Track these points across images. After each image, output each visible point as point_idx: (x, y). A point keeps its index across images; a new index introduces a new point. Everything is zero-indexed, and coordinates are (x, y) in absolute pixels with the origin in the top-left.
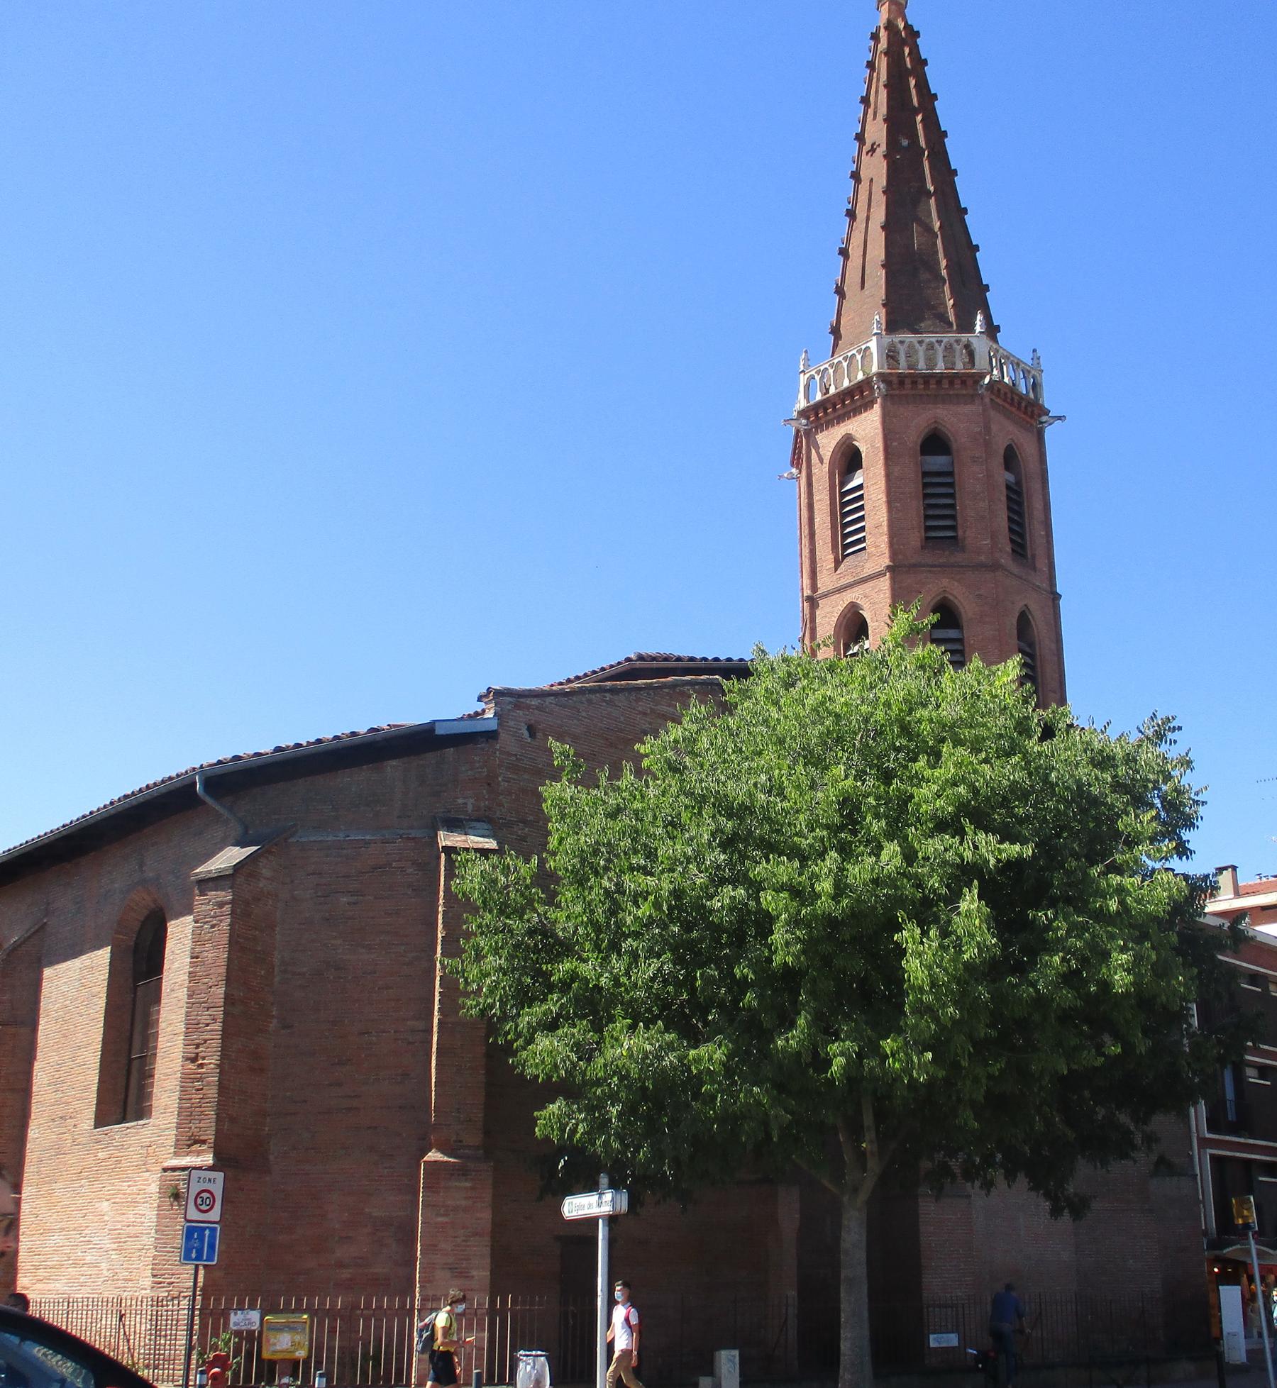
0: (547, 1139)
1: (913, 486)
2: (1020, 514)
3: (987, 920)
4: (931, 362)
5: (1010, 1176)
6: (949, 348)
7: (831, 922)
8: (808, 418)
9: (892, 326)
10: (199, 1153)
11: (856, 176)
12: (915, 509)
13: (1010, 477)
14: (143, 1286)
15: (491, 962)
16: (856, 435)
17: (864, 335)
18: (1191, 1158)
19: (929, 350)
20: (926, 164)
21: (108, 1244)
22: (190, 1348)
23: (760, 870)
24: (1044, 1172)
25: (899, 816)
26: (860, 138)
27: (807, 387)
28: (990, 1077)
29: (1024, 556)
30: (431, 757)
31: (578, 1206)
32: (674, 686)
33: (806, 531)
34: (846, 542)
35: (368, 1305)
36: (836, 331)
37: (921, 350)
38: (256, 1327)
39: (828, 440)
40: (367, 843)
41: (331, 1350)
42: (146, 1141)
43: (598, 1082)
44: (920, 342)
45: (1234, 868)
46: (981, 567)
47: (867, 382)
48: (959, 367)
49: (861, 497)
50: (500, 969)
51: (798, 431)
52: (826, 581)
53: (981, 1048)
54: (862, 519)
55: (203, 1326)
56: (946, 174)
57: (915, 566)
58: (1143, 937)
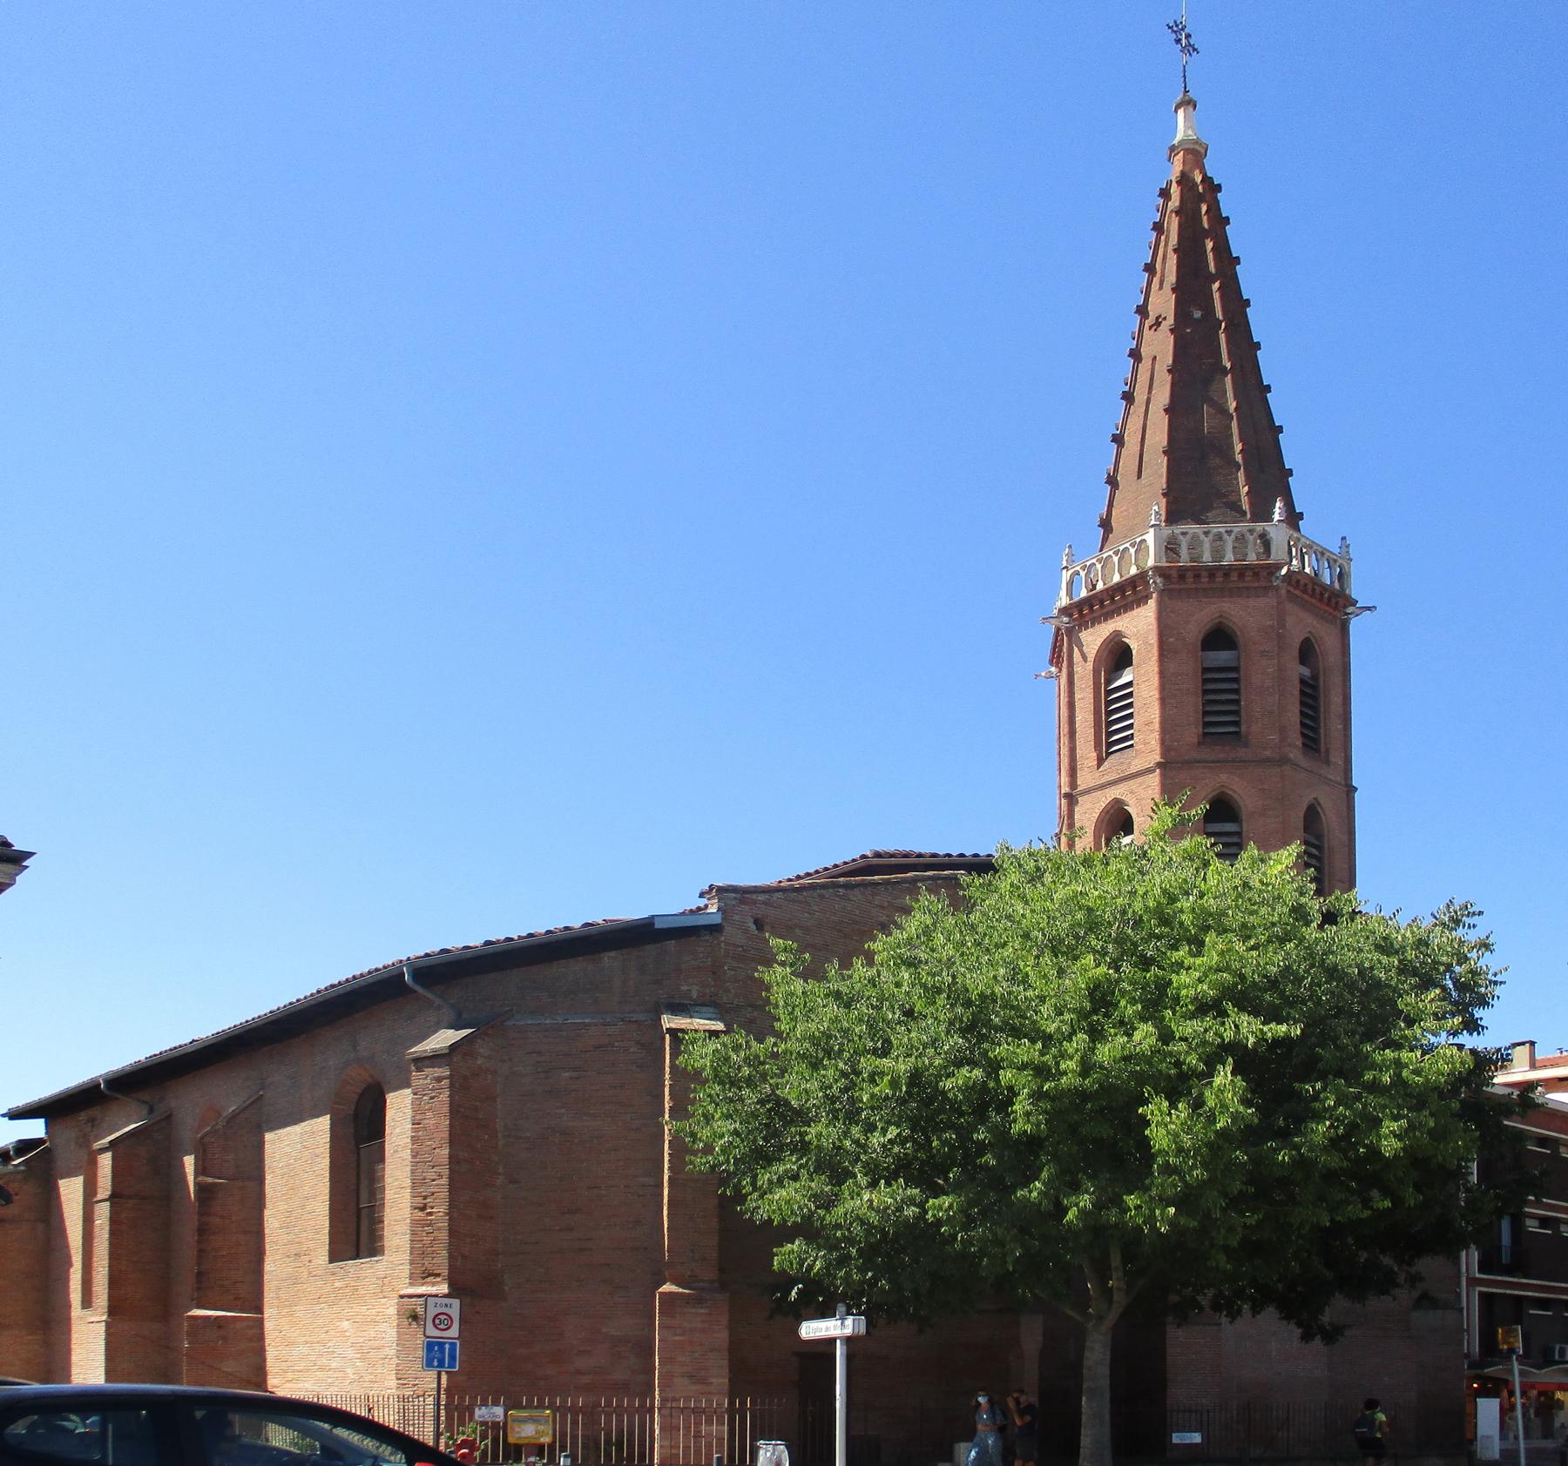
4: (1218, 553)
5: (1256, 1309)
6: (1241, 539)
8: (1070, 616)
9: (1173, 517)
10: (433, 1284)
11: (1135, 354)
12: (1192, 705)
13: (1306, 671)
18: (1459, 1295)
19: (1216, 541)
20: (1222, 337)
21: (350, 1353)
24: (1300, 1306)
25: (1156, 1001)
26: (1142, 311)
27: (1070, 584)
29: (1317, 750)
30: (651, 949)
31: (811, 1330)
33: (1065, 729)
36: (1106, 524)
37: (1207, 542)
39: (1093, 639)
40: (589, 1025)
41: (574, 1437)
43: (838, 1226)
44: (1206, 533)
45: (1532, 1044)
47: (1142, 576)
48: (1252, 558)
49: (1130, 695)
50: (736, 1133)
51: (1058, 629)
52: (1085, 779)
54: (1130, 716)
55: (449, 1418)
56: (1246, 348)
57: (1189, 762)
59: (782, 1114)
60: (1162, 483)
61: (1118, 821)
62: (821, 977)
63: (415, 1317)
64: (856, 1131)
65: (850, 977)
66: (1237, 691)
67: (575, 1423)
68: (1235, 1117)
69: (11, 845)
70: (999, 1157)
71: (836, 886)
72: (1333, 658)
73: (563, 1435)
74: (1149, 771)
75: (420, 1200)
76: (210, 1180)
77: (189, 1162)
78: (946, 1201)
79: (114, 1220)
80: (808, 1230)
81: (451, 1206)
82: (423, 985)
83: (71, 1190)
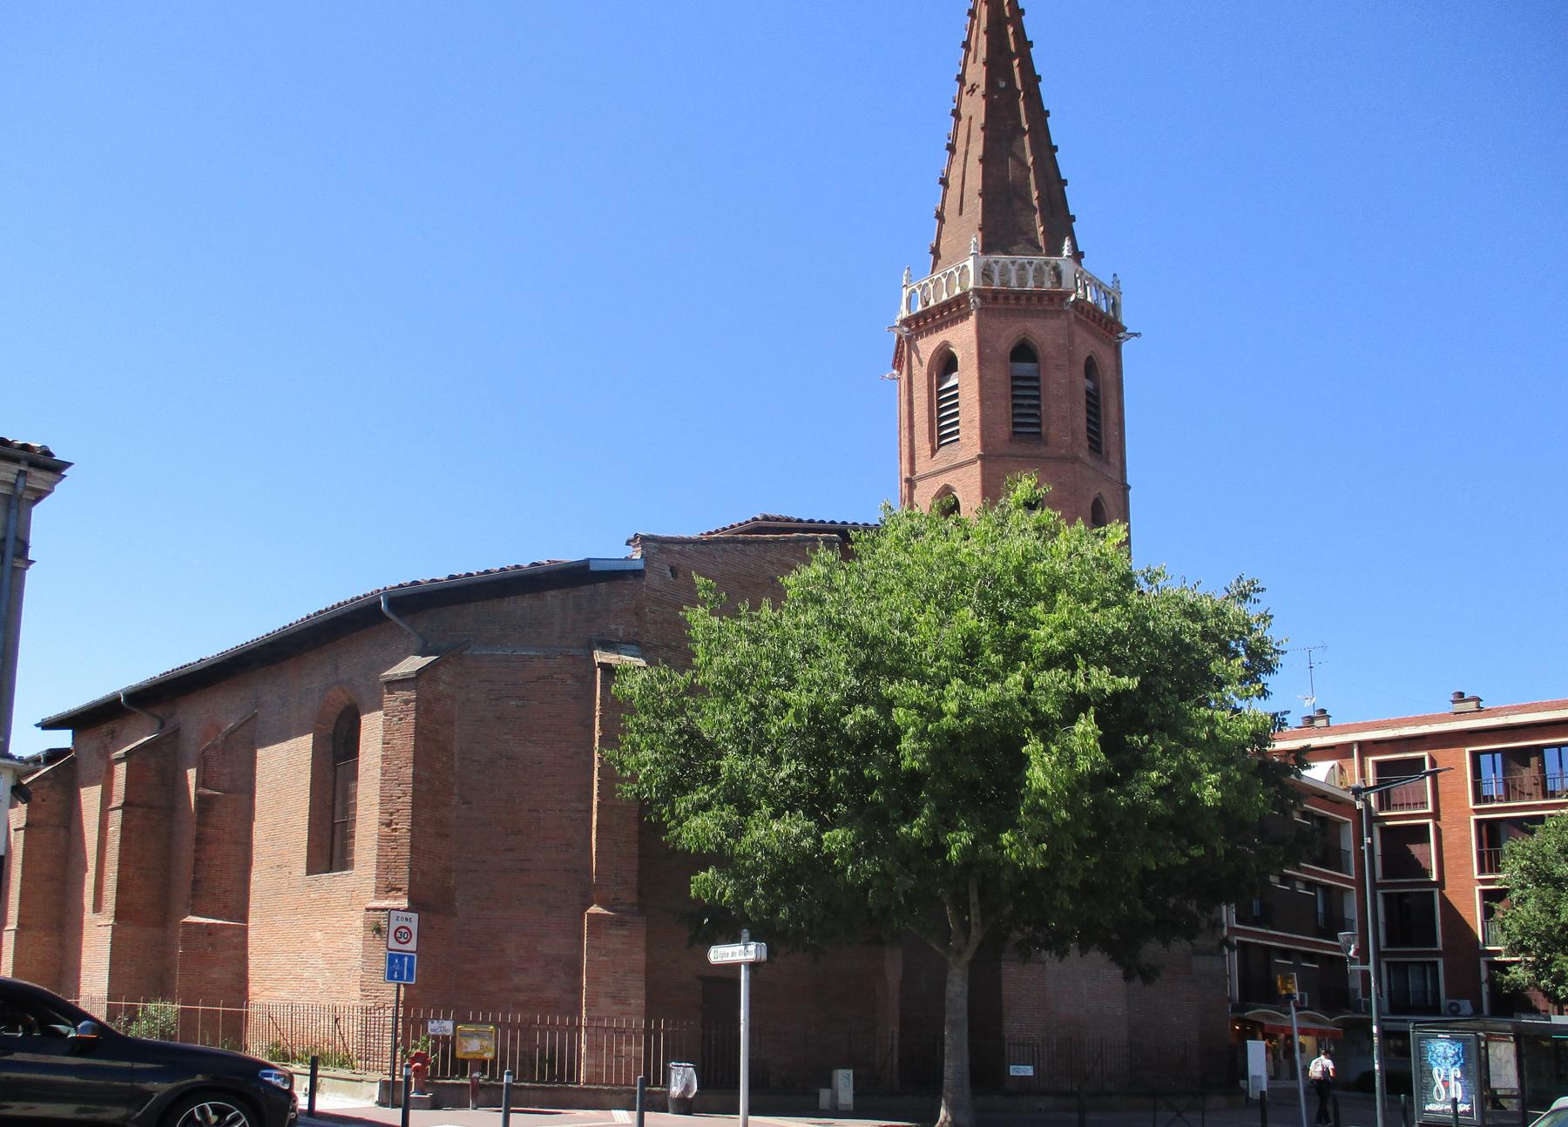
0: (698, 898)
1: (1003, 389)
2: (1097, 416)
3: (1100, 739)
4: (1022, 281)
5: (1084, 949)
6: (1039, 270)
7: (953, 736)
9: (987, 248)
10: (396, 898)
11: (956, 114)
12: (1004, 409)
13: (1090, 385)
14: (353, 997)
15: (647, 755)
16: (953, 342)
17: (964, 255)
19: (1021, 270)
20: (1022, 104)
21: (321, 963)
22: (396, 1046)
23: (891, 689)
24: (1122, 947)
25: (1014, 650)
26: (961, 79)
27: (909, 300)
28: (1086, 869)
29: (1099, 452)
30: (585, 591)
31: (720, 954)
32: (797, 540)
33: (905, 423)
34: (941, 434)
35: (543, 1021)
36: (936, 252)
37: (1013, 269)
38: (450, 1033)
39: (928, 346)
40: (531, 658)
41: (513, 1054)
42: (351, 887)
43: (745, 856)
46: (1062, 459)
47: (964, 297)
48: (1048, 286)
49: (956, 396)
50: (656, 762)
51: (900, 338)
52: (922, 466)
53: (1086, 846)
54: (956, 414)
55: (406, 1030)
56: (1039, 115)
57: (1001, 456)
58: (1228, 762)
59: (697, 747)
60: (979, 219)
61: (949, 506)
62: (735, 615)
63: (378, 930)
64: (762, 763)
65: (758, 618)
66: (1038, 398)
67: (514, 1039)
68: (1095, 763)
69: (52, 455)
70: (885, 794)
71: (735, 541)
72: (1108, 376)
73: (503, 1051)
74: (972, 462)
75: (387, 816)
76: (208, 792)
77: (192, 774)
78: (839, 833)
79: (124, 828)
80: (720, 859)
81: (413, 824)
82: (399, 616)
83: (90, 797)
